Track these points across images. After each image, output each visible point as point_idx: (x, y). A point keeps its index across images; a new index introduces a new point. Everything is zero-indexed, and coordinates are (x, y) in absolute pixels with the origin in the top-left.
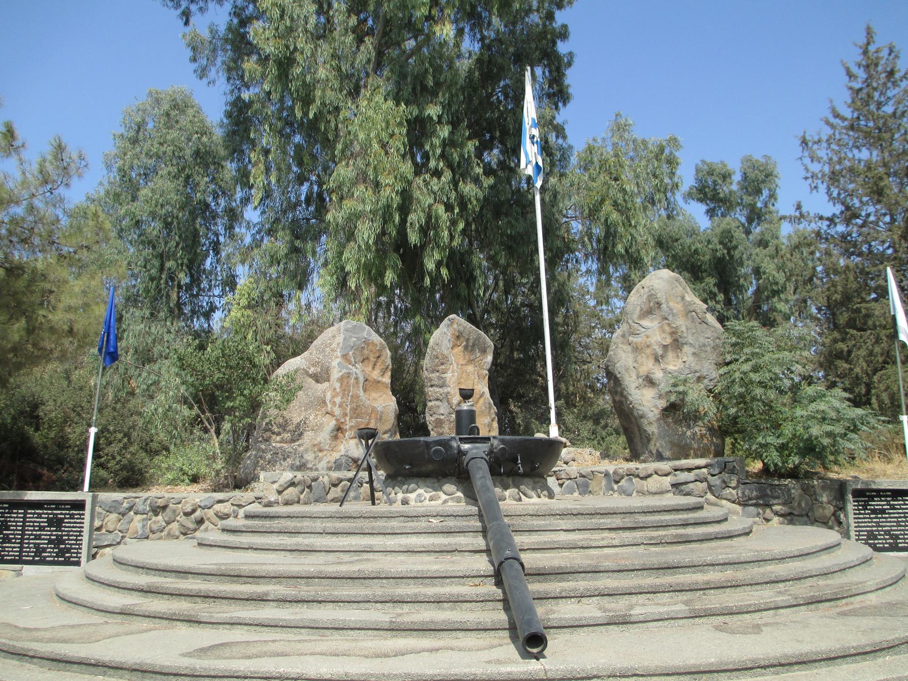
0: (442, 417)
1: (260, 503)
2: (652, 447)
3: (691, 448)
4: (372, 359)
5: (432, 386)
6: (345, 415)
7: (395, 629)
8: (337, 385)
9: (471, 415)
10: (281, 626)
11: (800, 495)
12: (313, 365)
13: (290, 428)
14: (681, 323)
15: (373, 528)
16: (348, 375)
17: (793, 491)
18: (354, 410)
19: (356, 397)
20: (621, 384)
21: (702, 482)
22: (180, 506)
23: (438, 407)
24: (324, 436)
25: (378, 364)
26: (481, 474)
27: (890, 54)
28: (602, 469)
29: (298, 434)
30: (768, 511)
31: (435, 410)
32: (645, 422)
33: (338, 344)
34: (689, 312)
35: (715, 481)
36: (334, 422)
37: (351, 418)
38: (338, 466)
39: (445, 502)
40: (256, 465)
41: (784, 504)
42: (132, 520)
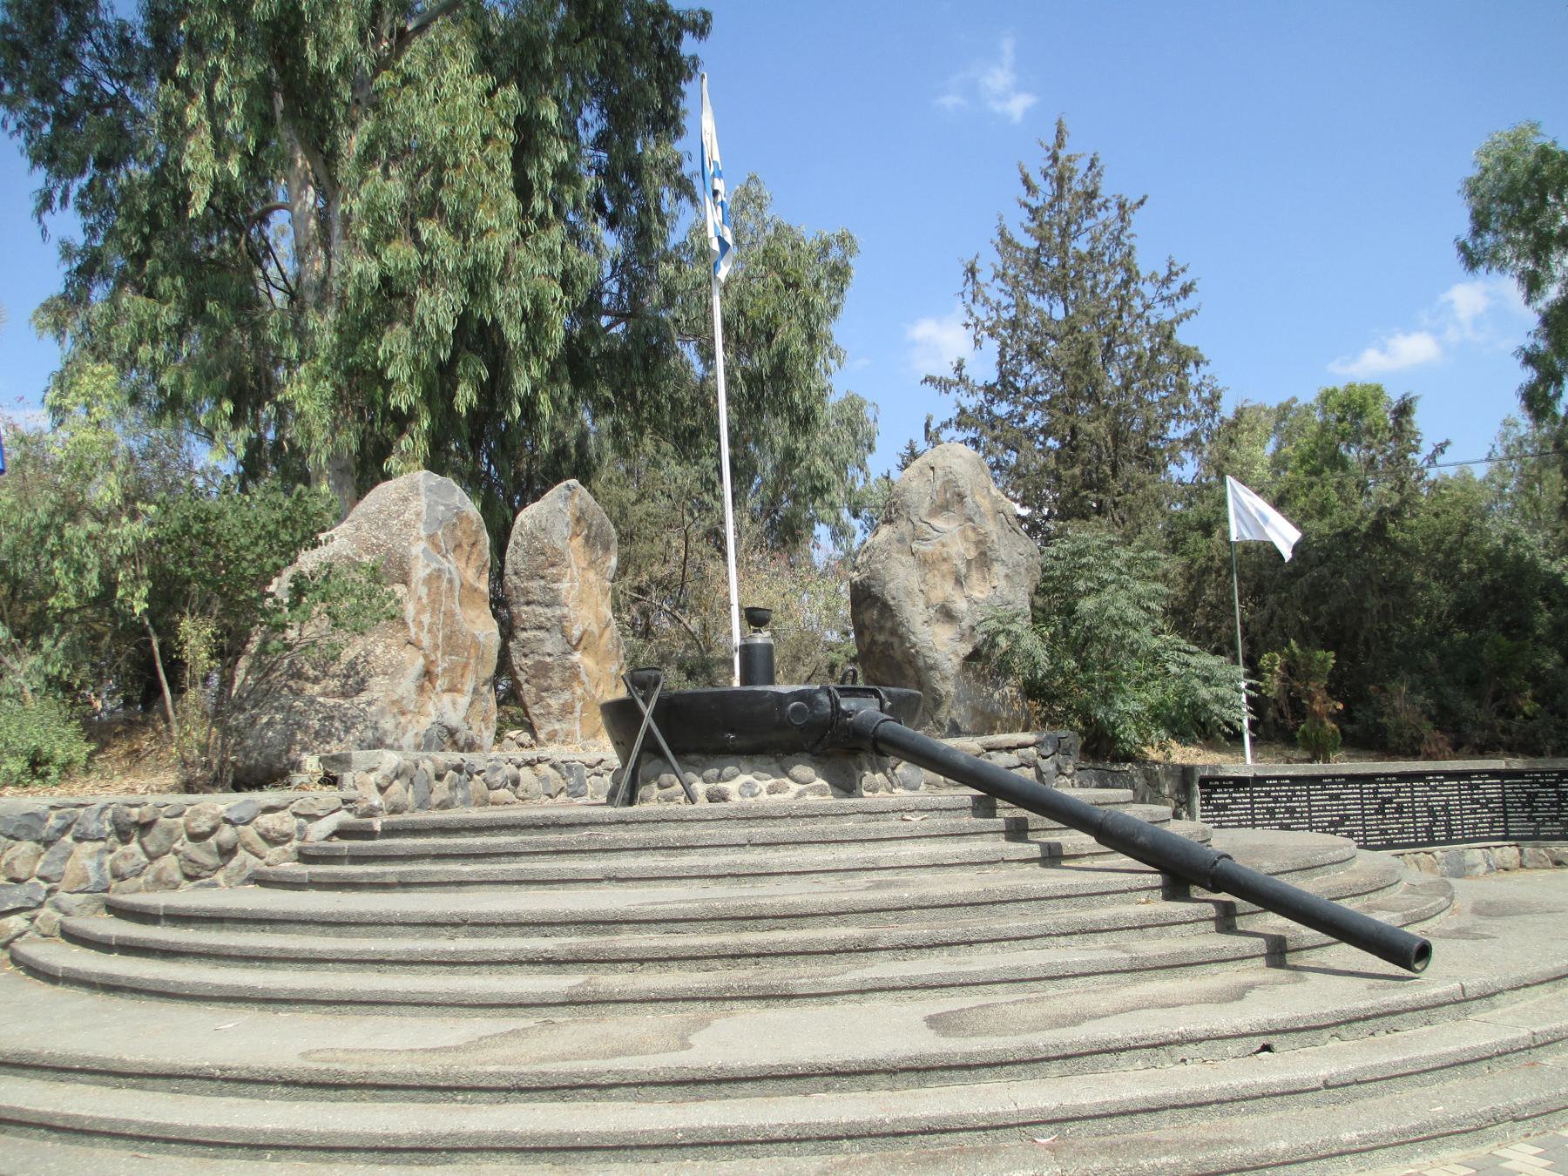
0: (548, 659)
1: (350, 810)
2: (942, 714)
5: (528, 603)
6: (436, 647)
7: (1140, 969)
8: (423, 591)
10: (962, 985)
12: (367, 551)
14: (991, 527)
15: (843, 832)
18: (448, 638)
19: (450, 615)
20: (893, 616)
22: (181, 820)
23: (541, 641)
24: (406, 686)
25: (474, 557)
27: (1090, 169)
29: (355, 682)
31: (534, 645)
33: (418, 514)
36: (420, 661)
39: (800, 794)
40: (290, 740)
42: (71, 853)
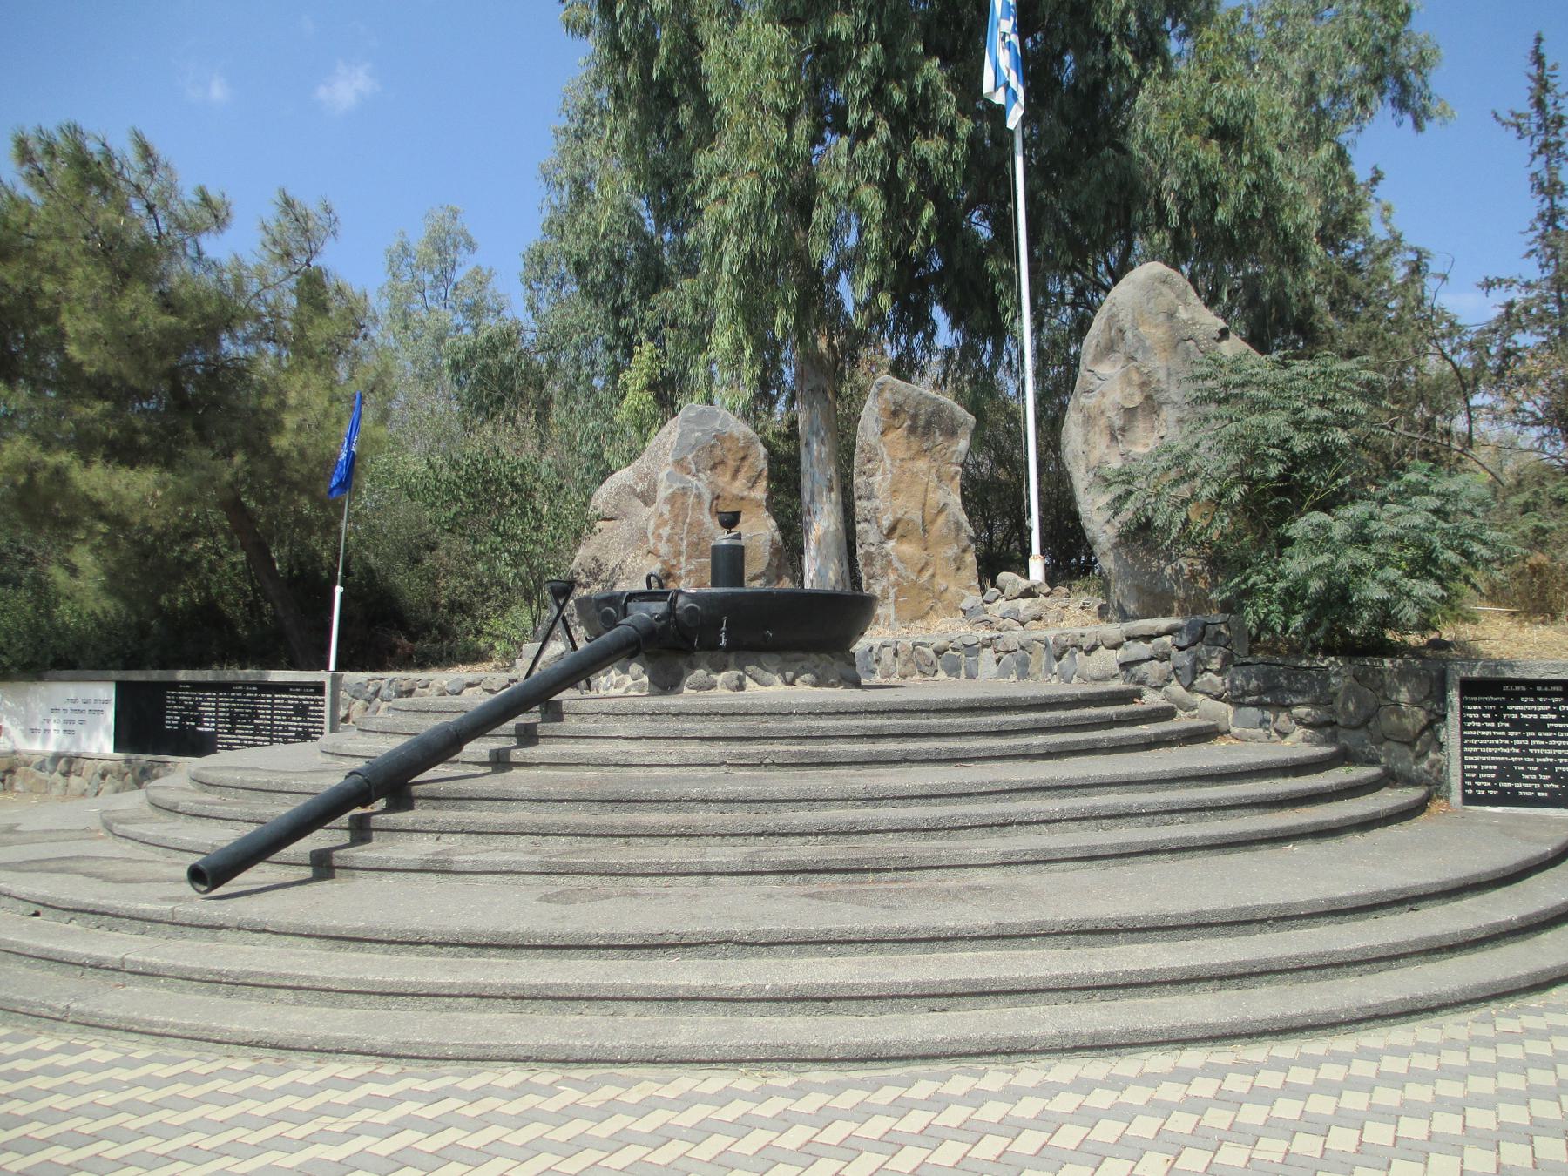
3: (1173, 598)
4: (732, 463)
8: (666, 509)
11: (1348, 688)
13: (604, 576)
14: (1158, 364)
16: (684, 491)
17: (1333, 680)
21: (1162, 660)
30: (1283, 716)
34: (1179, 340)
35: (1184, 659)
37: (689, 557)
41: (1314, 704)
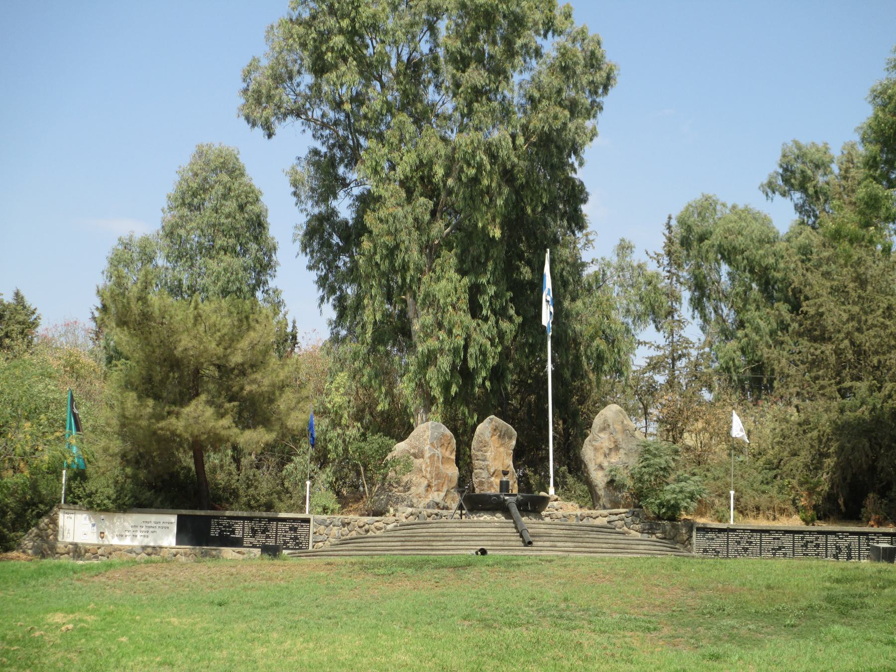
8: (428, 461)
9: (507, 482)
14: (619, 437)
16: (434, 455)
18: (437, 475)
24: (422, 490)
26: (514, 510)
28: (575, 513)
29: (407, 488)
32: (597, 489)
38: (428, 507)
40: (387, 504)
